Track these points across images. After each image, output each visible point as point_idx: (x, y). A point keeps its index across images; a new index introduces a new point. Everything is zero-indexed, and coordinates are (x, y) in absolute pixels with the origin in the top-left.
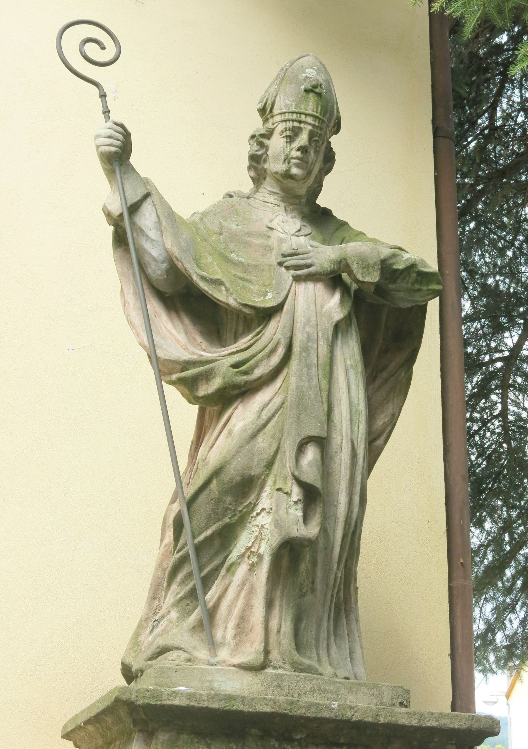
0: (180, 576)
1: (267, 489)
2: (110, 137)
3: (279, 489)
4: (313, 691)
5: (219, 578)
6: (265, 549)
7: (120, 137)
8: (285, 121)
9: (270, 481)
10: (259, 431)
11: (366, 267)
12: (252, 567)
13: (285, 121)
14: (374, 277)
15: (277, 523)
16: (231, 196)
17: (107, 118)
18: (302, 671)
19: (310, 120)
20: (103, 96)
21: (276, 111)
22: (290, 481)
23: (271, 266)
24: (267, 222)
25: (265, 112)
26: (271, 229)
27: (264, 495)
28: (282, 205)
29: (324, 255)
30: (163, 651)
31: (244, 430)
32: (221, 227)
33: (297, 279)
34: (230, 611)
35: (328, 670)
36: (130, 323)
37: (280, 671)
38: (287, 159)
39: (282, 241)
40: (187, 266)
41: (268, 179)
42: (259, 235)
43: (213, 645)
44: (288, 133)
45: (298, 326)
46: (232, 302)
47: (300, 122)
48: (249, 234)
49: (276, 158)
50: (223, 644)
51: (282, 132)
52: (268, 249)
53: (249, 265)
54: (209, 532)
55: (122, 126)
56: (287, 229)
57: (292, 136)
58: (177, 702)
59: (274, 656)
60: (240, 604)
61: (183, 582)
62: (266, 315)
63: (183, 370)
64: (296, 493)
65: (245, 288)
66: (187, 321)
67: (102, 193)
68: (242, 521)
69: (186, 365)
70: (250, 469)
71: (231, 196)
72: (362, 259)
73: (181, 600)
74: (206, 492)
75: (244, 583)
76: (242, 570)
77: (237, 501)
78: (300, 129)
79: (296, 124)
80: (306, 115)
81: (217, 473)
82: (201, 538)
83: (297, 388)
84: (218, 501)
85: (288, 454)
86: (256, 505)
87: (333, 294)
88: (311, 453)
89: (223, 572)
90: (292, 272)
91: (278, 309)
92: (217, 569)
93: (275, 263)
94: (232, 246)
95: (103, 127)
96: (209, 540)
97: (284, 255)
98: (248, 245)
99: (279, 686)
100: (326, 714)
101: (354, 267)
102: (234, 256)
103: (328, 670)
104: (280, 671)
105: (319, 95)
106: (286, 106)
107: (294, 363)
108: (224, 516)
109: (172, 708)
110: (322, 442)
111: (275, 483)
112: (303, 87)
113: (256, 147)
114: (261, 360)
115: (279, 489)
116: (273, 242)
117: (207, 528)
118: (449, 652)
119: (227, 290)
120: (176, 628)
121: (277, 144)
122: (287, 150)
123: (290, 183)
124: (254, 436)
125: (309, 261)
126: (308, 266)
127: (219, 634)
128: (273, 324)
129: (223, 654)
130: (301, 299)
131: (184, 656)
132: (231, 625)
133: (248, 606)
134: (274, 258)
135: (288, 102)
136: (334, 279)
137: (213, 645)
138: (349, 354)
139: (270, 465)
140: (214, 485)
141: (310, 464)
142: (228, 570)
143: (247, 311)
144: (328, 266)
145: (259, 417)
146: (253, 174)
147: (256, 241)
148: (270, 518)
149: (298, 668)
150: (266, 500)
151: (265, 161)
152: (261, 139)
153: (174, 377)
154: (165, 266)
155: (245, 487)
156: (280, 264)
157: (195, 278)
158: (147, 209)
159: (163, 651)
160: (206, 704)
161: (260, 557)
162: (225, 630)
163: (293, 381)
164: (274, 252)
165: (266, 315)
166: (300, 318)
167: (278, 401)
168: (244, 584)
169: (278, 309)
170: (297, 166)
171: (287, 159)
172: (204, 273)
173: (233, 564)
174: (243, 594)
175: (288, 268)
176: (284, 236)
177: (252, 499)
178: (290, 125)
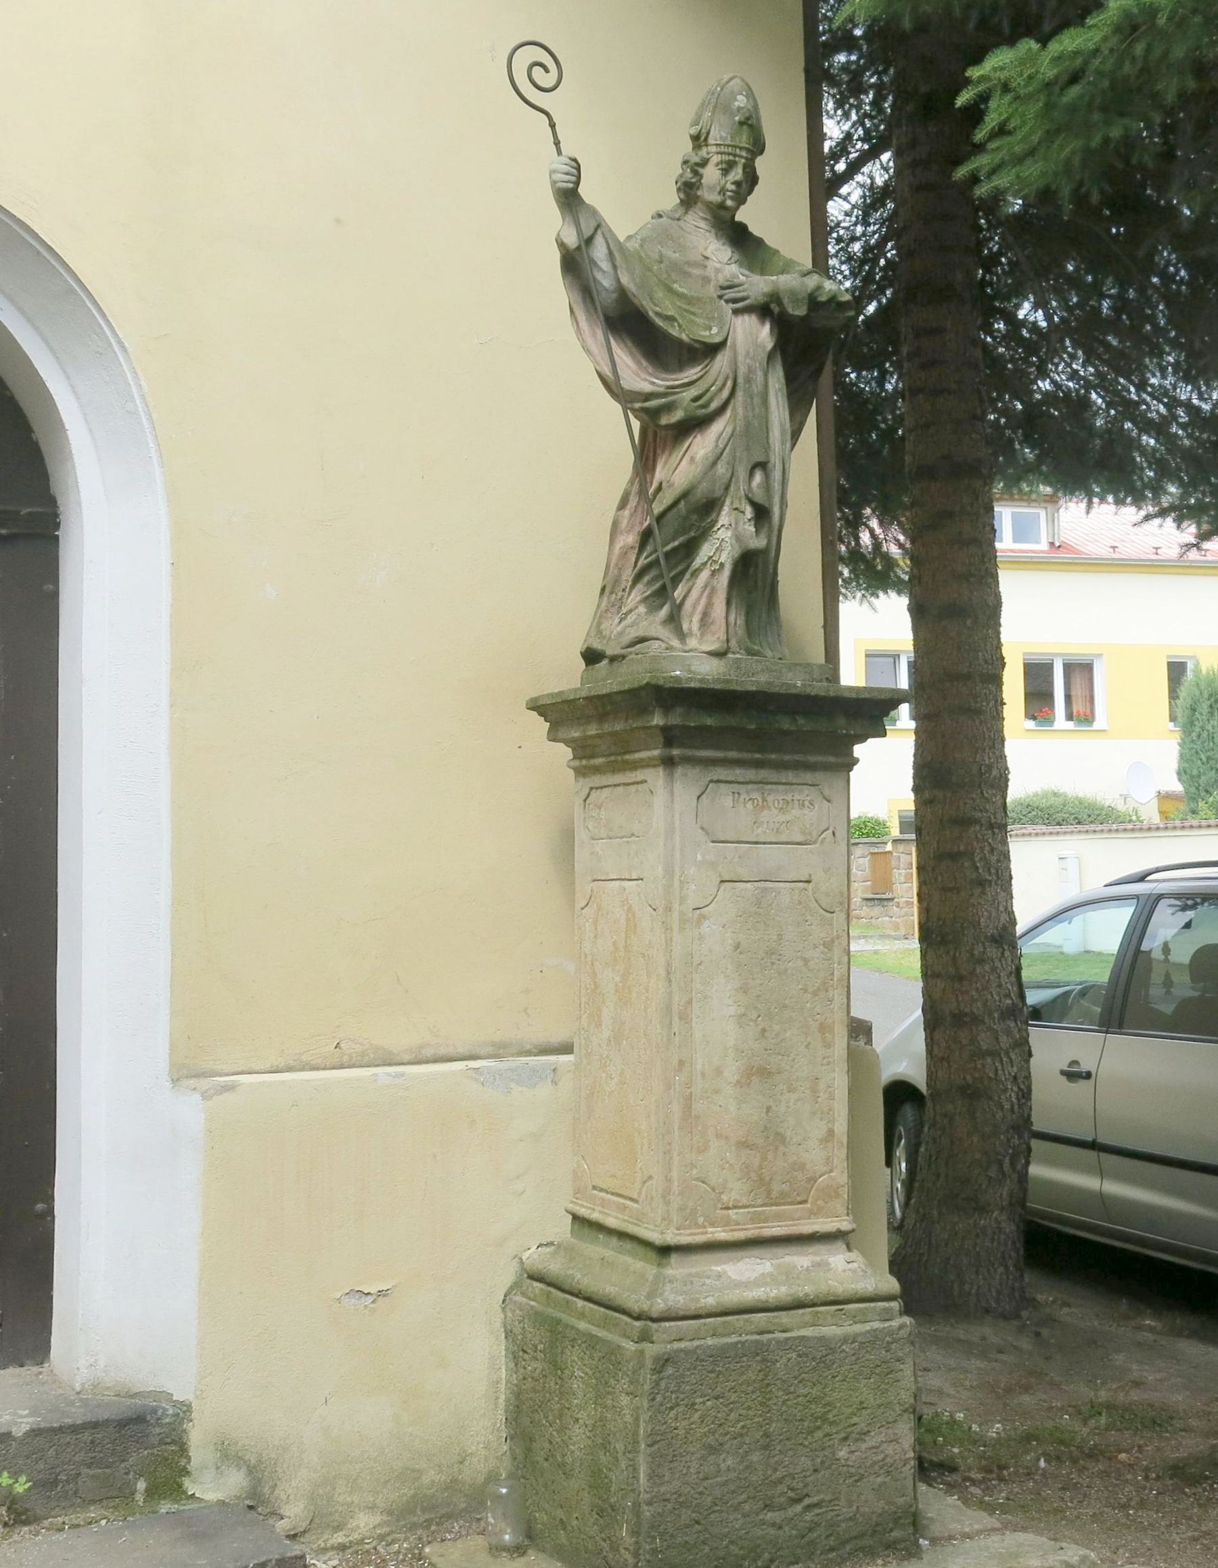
0: (646, 579)
1: (726, 509)
2: (567, 174)
3: (736, 509)
4: (763, 670)
5: (684, 580)
6: (727, 557)
7: (575, 171)
8: (721, 153)
9: (728, 502)
10: (718, 459)
11: (796, 301)
12: (714, 573)
13: (721, 153)
14: (801, 311)
15: (738, 538)
16: (660, 216)
17: (559, 152)
18: (753, 655)
19: (744, 154)
20: (553, 126)
21: (711, 141)
22: (744, 501)
23: (711, 299)
24: (701, 250)
25: (698, 140)
26: (707, 258)
27: (723, 513)
28: (713, 231)
29: (758, 286)
30: (642, 640)
31: (706, 457)
32: (661, 256)
33: (736, 312)
34: (694, 607)
35: (769, 653)
36: (588, 351)
37: (738, 656)
38: (723, 191)
39: (717, 271)
40: (644, 303)
41: (699, 204)
42: (696, 264)
43: (682, 636)
44: (724, 166)
45: (740, 358)
46: (684, 337)
47: (735, 155)
48: (688, 263)
49: (711, 189)
50: (691, 634)
51: (718, 164)
52: (706, 280)
53: (692, 297)
54: (676, 543)
55: (575, 160)
56: (719, 257)
57: (727, 168)
58: (692, 685)
59: (733, 643)
60: (703, 602)
61: (649, 583)
62: (712, 350)
63: (646, 400)
64: (749, 512)
65: (692, 321)
66: (630, 344)
67: (552, 223)
68: (704, 534)
69: (649, 396)
70: (713, 492)
71: (660, 216)
72: (793, 293)
73: (647, 598)
74: (675, 510)
75: (706, 586)
76: (704, 575)
77: (702, 519)
78: (735, 162)
79: (731, 158)
80: (741, 148)
81: (685, 495)
82: (669, 547)
83: (746, 417)
84: (686, 518)
85: (741, 478)
86: (716, 521)
87: (763, 324)
88: (758, 477)
89: (687, 576)
90: (731, 305)
91: (723, 344)
92: (681, 575)
93: (715, 296)
94: (674, 276)
95: (561, 164)
96: (674, 550)
97: (723, 288)
98: (689, 275)
99: (738, 668)
100: (793, 691)
101: (785, 301)
102: (675, 286)
103: (769, 653)
104: (738, 656)
105: (751, 126)
106: (721, 138)
107: (740, 395)
108: (690, 530)
109: (690, 689)
110: (763, 465)
111: (732, 503)
112: (737, 118)
113: (689, 174)
114: (715, 394)
115: (736, 509)
116: (710, 272)
117: (674, 540)
118: (822, 624)
119: (680, 326)
120: (639, 618)
121: (711, 174)
122: (723, 182)
123: (723, 213)
124: (714, 463)
125: (745, 294)
126: (743, 299)
127: (685, 627)
128: (719, 357)
129: (692, 643)
130: (739, 331)
131: (664, 645)
132: (696, 619)
133: (709, 604)
134: (712, 290)
135: (724, 134)
136: (765, 310)
137: (682, 636)
138: (777, 379)
139: (727, 488)
140: (682, 504)
141: (758, 486)
142: (692, 575)
143: (697, 345)
144: (761, 299)
145: (717, 446)
146: (682, 196)
147: (696, 271)
148: (729, 533)
149: (750, 652)
150: (725, 517)
151: (698, 189)
152: (696, 168)
153: (637, 405)
154: (614, 295)
155: (709, 507)
156: (720, 297)
157: (651, 314)
158: (599, 241)
159: (642, 640)
160: (712, 686)
161: (722, 565)
162: (691, 623)
163: (740, 411)
164: (713, 283)
165: (712, 350)
166: (741, 351)
167: (729, 430)
168: (706, 588)
169: (723, 344)
170: (731, 198)
171: (723, 191)
172: (657, 309)
173: (696, 570)
174: (706, 594)
175: (727, 301)
176: (718, 265)
177: (714, 516)
178: (726, 158)
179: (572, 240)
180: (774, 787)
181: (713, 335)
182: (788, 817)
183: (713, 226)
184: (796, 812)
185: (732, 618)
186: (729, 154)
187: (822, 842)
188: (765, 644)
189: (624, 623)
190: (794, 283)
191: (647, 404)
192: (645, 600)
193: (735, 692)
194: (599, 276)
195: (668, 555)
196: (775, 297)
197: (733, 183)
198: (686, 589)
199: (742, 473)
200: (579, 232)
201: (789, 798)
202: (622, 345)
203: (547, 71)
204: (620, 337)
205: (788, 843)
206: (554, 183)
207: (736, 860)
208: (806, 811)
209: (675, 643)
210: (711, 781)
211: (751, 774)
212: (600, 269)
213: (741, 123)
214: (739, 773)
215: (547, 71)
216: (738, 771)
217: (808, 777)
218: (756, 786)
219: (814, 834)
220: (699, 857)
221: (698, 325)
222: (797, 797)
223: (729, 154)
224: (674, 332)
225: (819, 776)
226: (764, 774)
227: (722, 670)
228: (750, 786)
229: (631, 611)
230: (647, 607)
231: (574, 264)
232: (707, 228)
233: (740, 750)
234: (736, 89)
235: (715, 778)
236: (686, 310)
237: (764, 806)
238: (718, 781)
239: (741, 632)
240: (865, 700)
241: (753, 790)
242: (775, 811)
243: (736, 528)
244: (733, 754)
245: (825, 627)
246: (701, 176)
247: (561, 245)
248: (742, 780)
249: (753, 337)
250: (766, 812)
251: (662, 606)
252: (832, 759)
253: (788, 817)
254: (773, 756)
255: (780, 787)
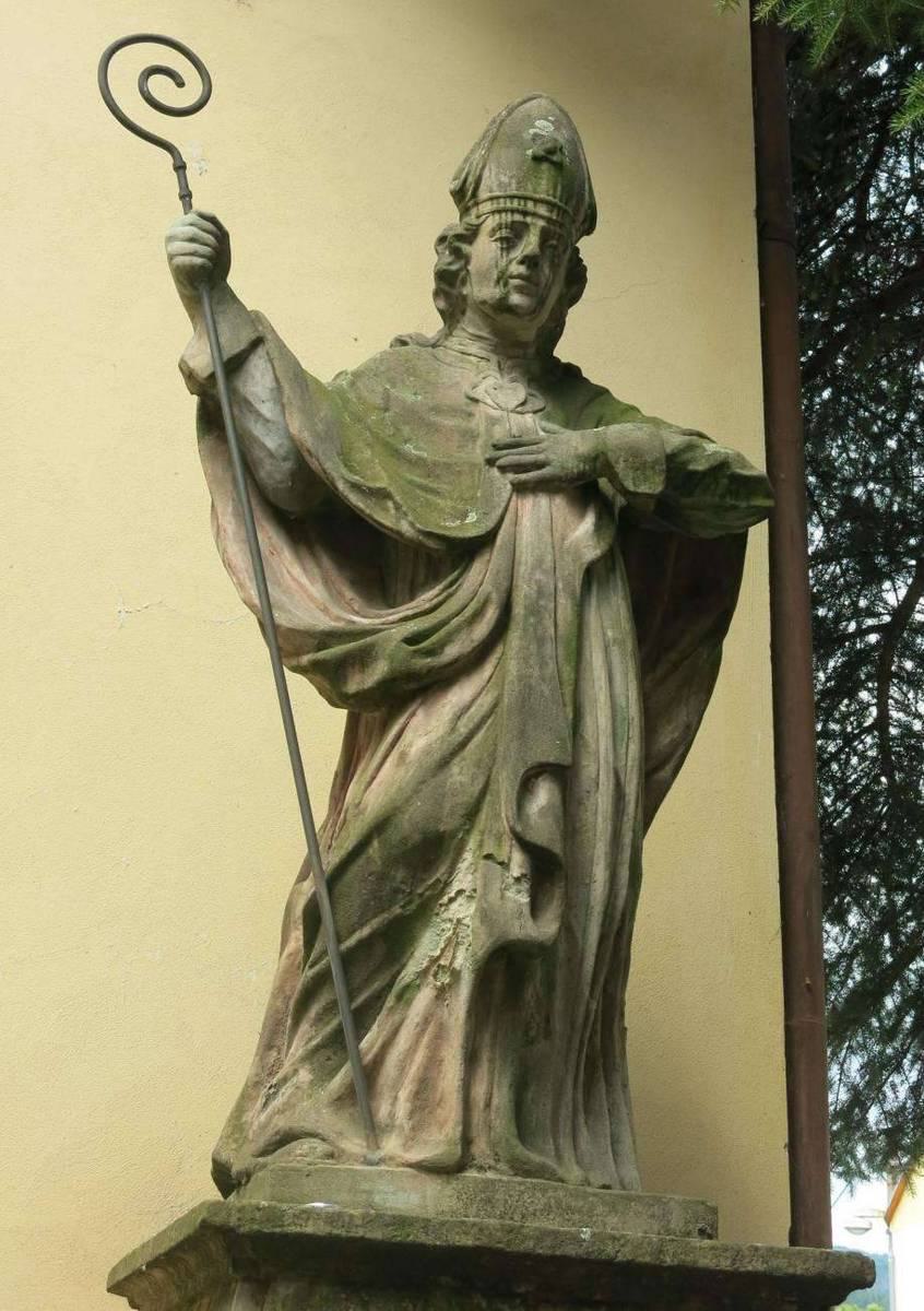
1: (468, 857)
2: (192, 240)
3: (488, 857)
5: (384, 1011)
7: (210, 239)
8: (499, 212)
9: (472, 844)
12: (442, 993)
14: (653, 485)
15: (485, 916)
16: (404, 343)
17: (188, 207)
18: (528, 1174)
19: (542, 210)
20: (180, 167)
21: (483, 194)
23: (473, 465)
24: (466, 388)
25: (464, 196)
26: (476, 401)
27: (463, 866)
29: (568, 446)
31: (427, 751)
32: (387, 397)
33: (520, 489)
35: (574, 1173)
36: (228, 565)
37: (490, 1175)
38: (503, 279)
40: (328, 465)
41: (469, 313)
42: (454, 411)
43: (373, 1130)
44: (504, 233)
45: (522, 570)
46: (405, 527)
48: (437, 410)
49: (484, 276)
50: (389, 1128)
51: (493, 231)
52: (471, 436)
53: (435, 464)
54: (365, 931)
55: (213, 220)
56: (500, 400)
58: (309, 1229)
59: (480, 1147)
60: (420, 1056)
61: (319, 1019)
62: (466, 551)
63: (321, 647)
64: (518, 863)
66: (326, 562)
67: (176, 336)
68: (424, 910)
69: (327, 638)
70: (439, 820)
71: (404, 343)
73: (317, 1048)
74: (361, 861)
76: (423, 999)
78: (526, 226)
79: (518, 217)
80: (536, 201)
81: (380, 827)
84: (382, 877)
85: (503, 796)
86: (447, 884)
87: (582, 516)
88: (544, 795)
89: (390, 1001)
90: (511, 476)
91: (486, 541)
92: (378, 999)
94: (406, 430)
95: (179, 222)
96: (365, 944)
97: (496, 447)
98: (433, 428)
99: (489, 1201)
100: (571, 1250)
101: (620, 467)
102: (409, 448)
103: (574, 1173)
104: (490, 1175)
105: (559, 166)
106: (500, 184)
107: (514, 638)
108: (392, 903)
110: (564, 775)
111: (481, 845)
112: (530, 152)
113: (448, 258)
115: (488, 857)
119: (398, 507)
120: (308, 1100)
121: (484, 251)
122: (503, 263)
123: (507, 320)
124: (444, 763)
125: (541, 457)
126: (539, 466)
127: (383, 1111)
129: (391, 1145)
130: (526, 522)
131: (321, 1147)
132: (404, 1094)
133: (433, 1063)
134: (479, 453)
135: (504, 179)
136: (583, 488)
137: (373, 1130)
139: (472, 813)
140: (375, 848)
141: (543, 812)
142: (399, 997)
143: (431, 544)
144: (574, 466)
145: (453, 729)
147: (449, 422)
148: (473, 907)
149: (521, 1169)
151: (464, 282)
152: (456, 244)
153: (305, 659)
154: (288, 465)
156: (490, 462)
157: (341, 486)
159: (286, 1138)
160: (360, 1233)
162: (395, 1104)
163: (513, 667)
164: (480, 442)
165: (466, 551)
167: (486, 701)
169: (486, 541)
170: (520, 290)
171: (503, 279)
173: (407, 987)
174: (425, 1040)
175: (503, 469)
176: (496, 413)
178: (508, 218)
179: (203, 362)
181: (472, 525)
183: (496, 349)
185: (479, 1091)
186: (513, 211)
188: (568, 1154)
189: (270, 1109)
190: (639, 434)
191: (321, 655)
192: (310, 1056)
193: (421, 1248)
194: (258, 430)
195: (347, 960)
196: (599, 463)
197: (522, 262)
198: (388, 1028)
199: (505, 786)
200: (217, 346)
202: (311, 565)
203: (181, 84)
204: (313, 554)
206: (171, 257)
209: (354, 1144)
212: (259, 415)
213: (537, 159)
215: (181, 84)
221: (442, 510)
223: (513, 211)
224: (385, 517)
227: (454, 1203)
229: (285, 1080)
230: (312, 1071)
231: (216, 412)
232: (484, 354)
234: (535, 113)
236: (421, 487)
239: (502, 1123)
240: (754, 1277)
243: (485, 895)
245: (793, 1147)
246: (467, 259)
247: (189, 375)
249: (553, 537)
251: (336, 1070)
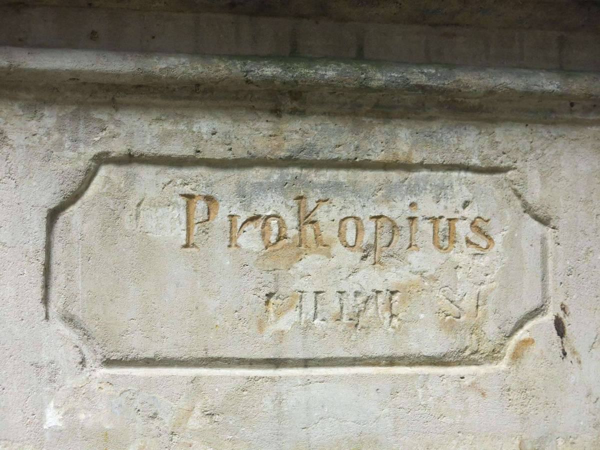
180: (342, 175)
182: (394, 276)
184: (425, 259)
187: (516, 356)
201: (398, 210)
205: (392, 361)
207: (195, 422)
208: (461, 255)
210: (102, 159)
211: (254, 134)
214: (208, 131)
216: (204, 125)
217: (471, 143)
218: (275, 175)
219: (491, 329)
220: (53, 418)
222: (427, 206)
225: (509, 140)
226: (297, 133)
228: (256, 175)
233: (197, 51)
235: (118, 148)
237: (307, 236)
238: (130, 159)
241: (262, 188)
242: (348, 258)
244: (221, 69)
248: (220, 152)
250: (312, 261)
252: (548, 83)
253: (394, 276)
254: (330, 73)
255: (369, 177)
